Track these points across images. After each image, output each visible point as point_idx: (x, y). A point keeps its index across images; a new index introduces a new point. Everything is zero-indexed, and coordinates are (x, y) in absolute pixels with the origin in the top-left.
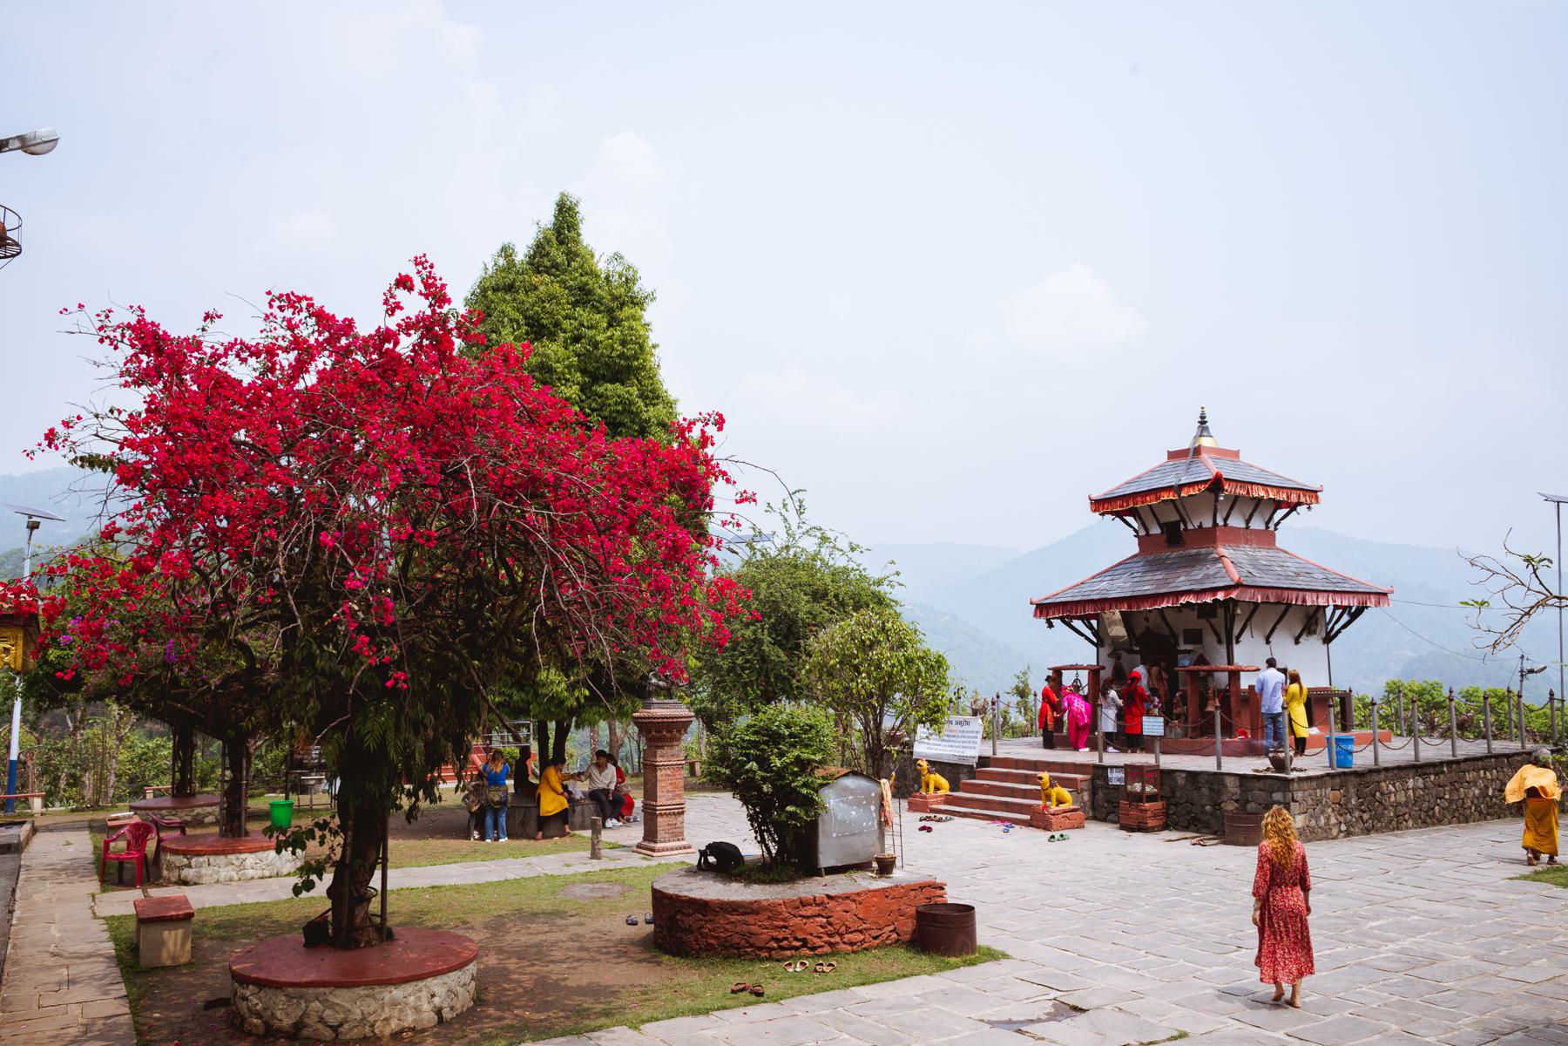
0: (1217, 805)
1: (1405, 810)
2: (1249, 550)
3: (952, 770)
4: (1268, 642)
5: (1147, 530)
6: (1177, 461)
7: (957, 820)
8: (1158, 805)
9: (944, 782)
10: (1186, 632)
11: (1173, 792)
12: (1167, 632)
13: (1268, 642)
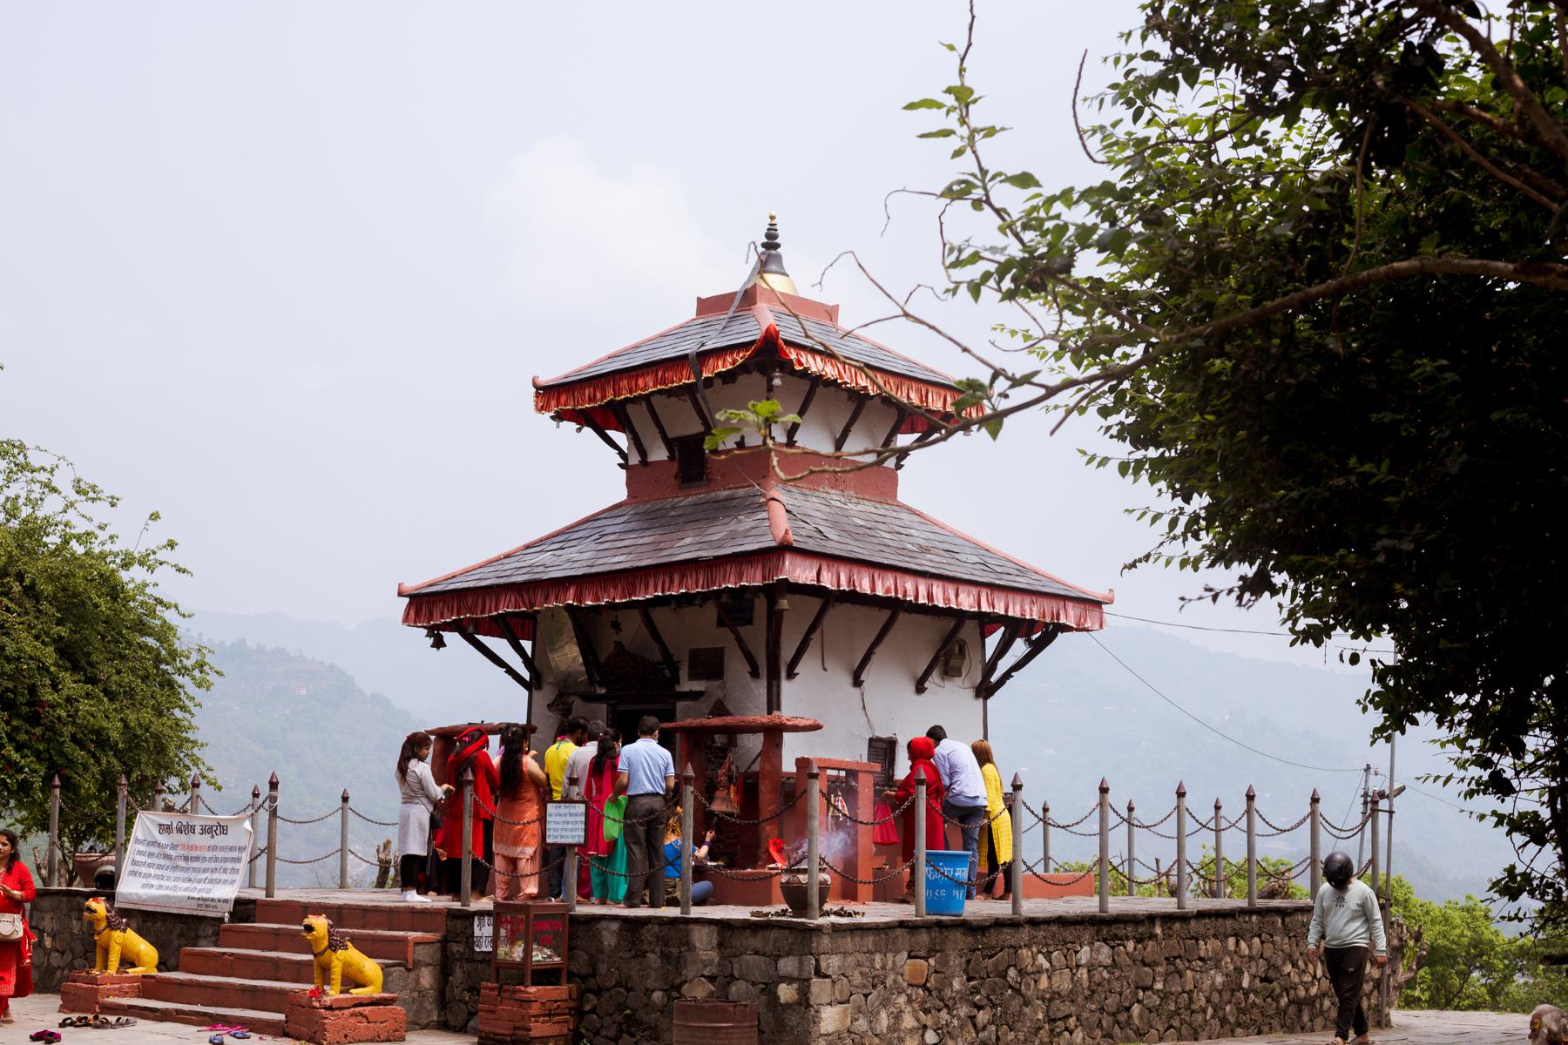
0: (674, 988)
1: (1068, 1008)
2: (835, 497)
3: (172, 929)
4: (857, 683)
5: (643, 453)
6: (711, 318)
7: (143, 1025)
8: (561, 991)
9: (147, 951)
10: (694, 654)
11: (593, 964)
12: (657, 656)
13: (857, 683)
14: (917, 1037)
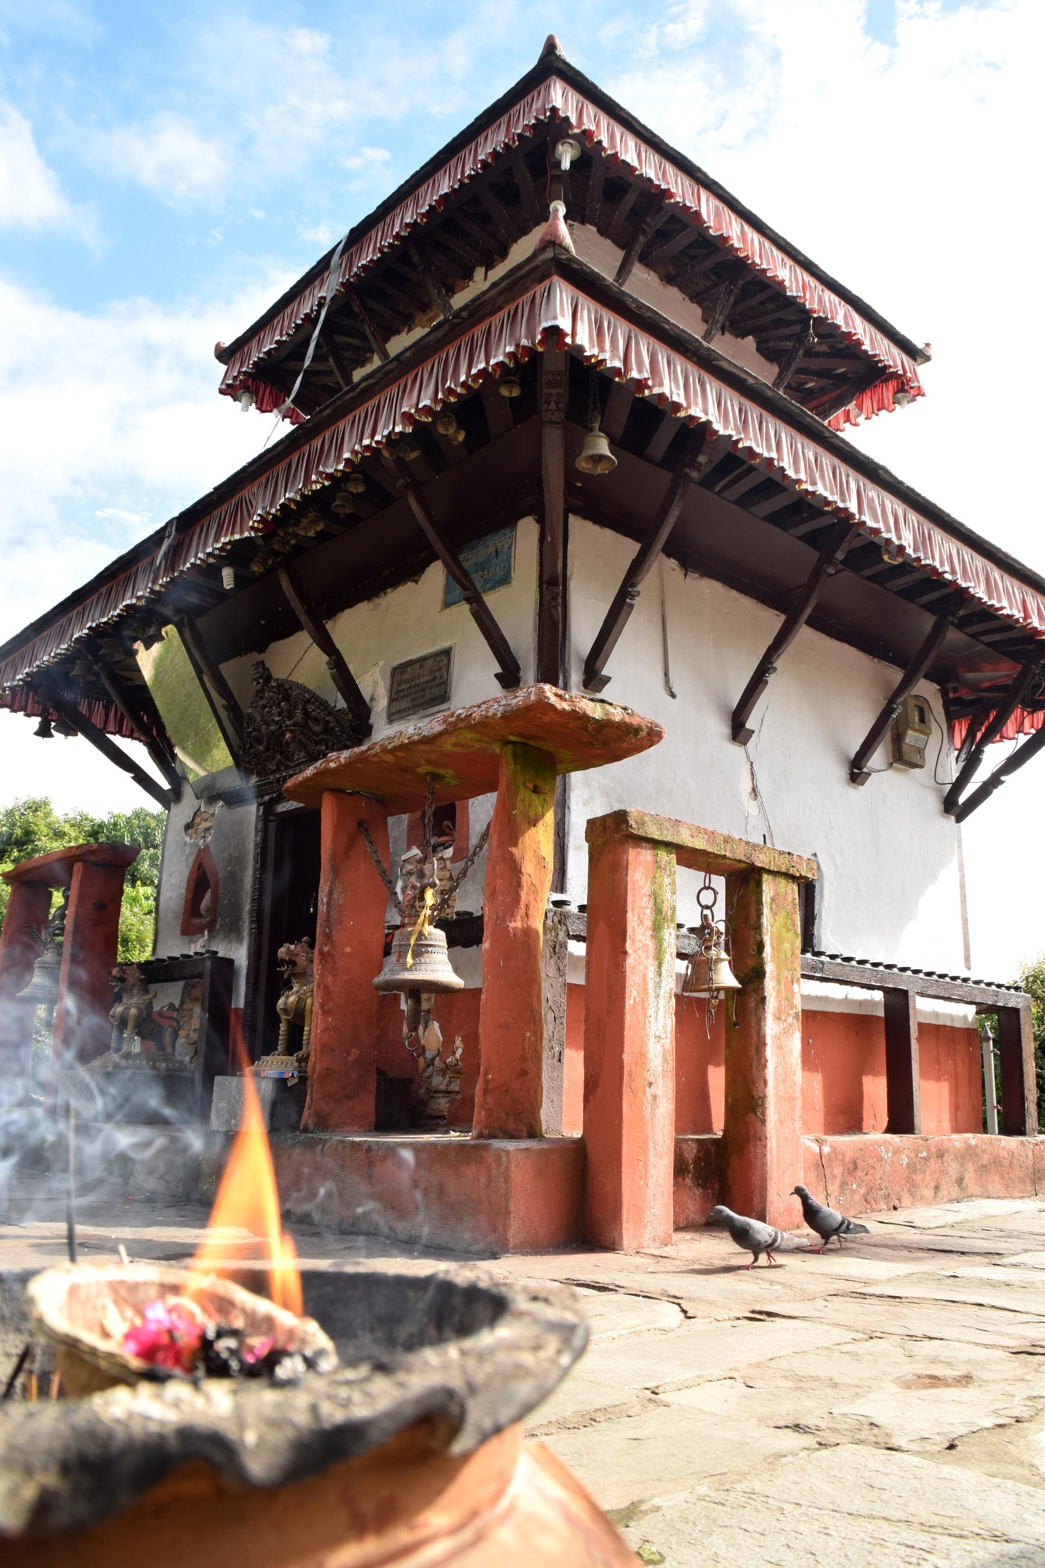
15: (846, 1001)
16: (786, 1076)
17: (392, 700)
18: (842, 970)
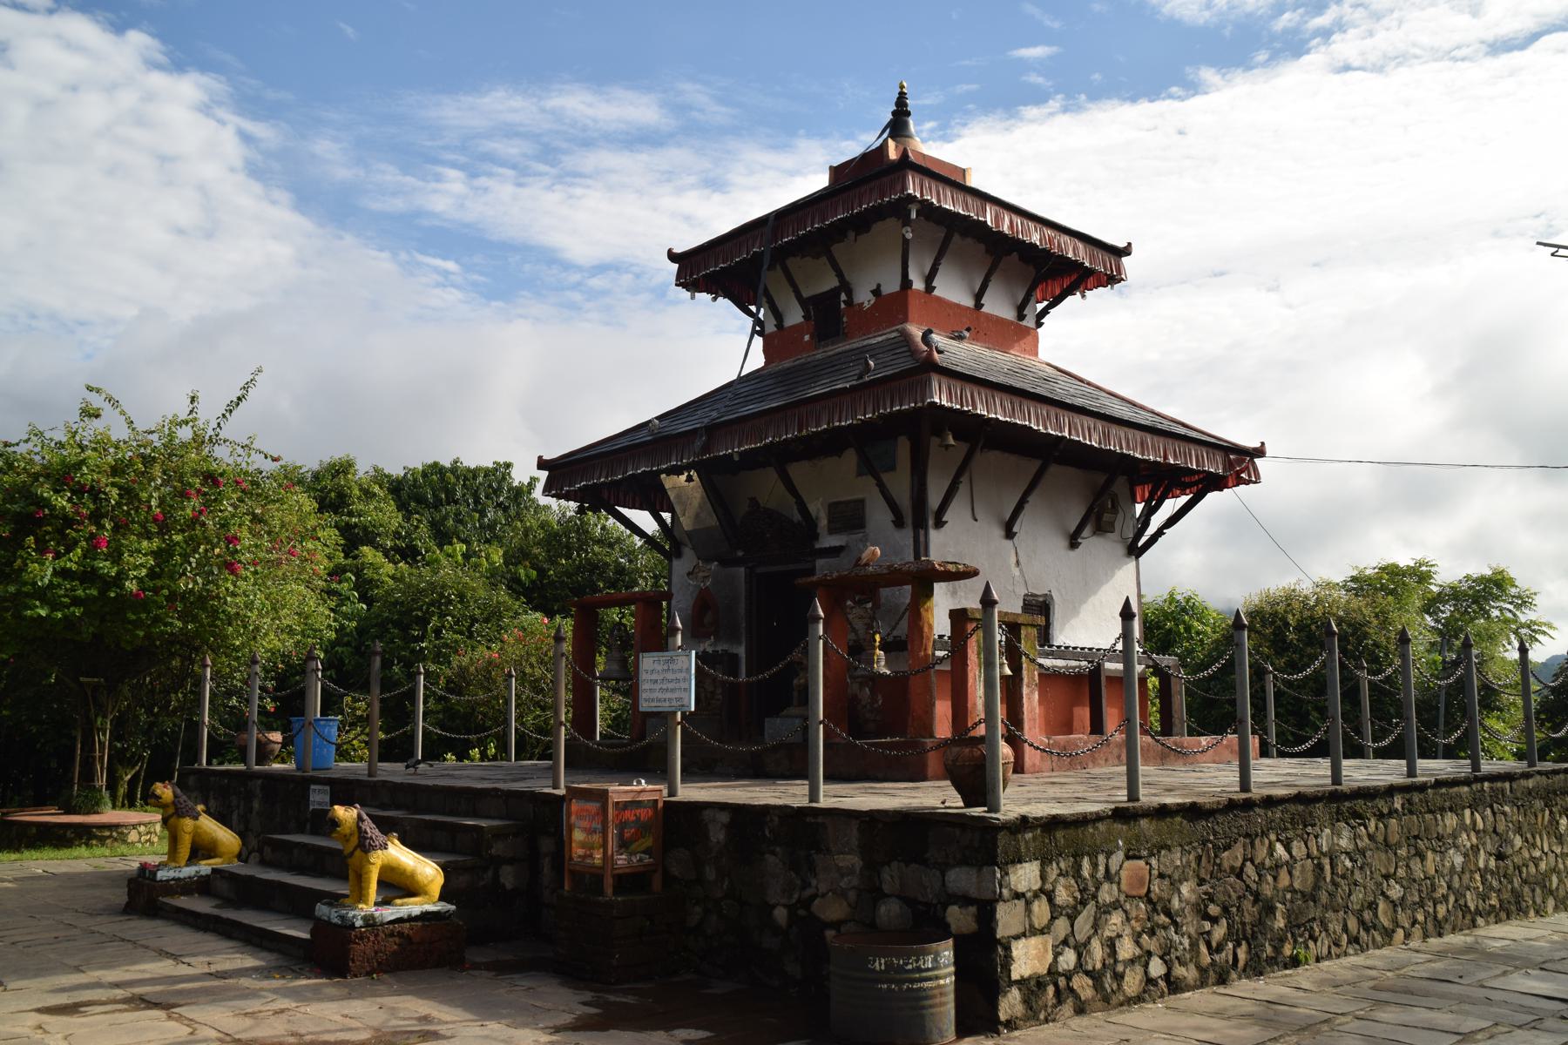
14: (1139, 969)
15: (1067, 667)
16: (1032, 710)
17: (829, 522)
18: (1065, 652)
